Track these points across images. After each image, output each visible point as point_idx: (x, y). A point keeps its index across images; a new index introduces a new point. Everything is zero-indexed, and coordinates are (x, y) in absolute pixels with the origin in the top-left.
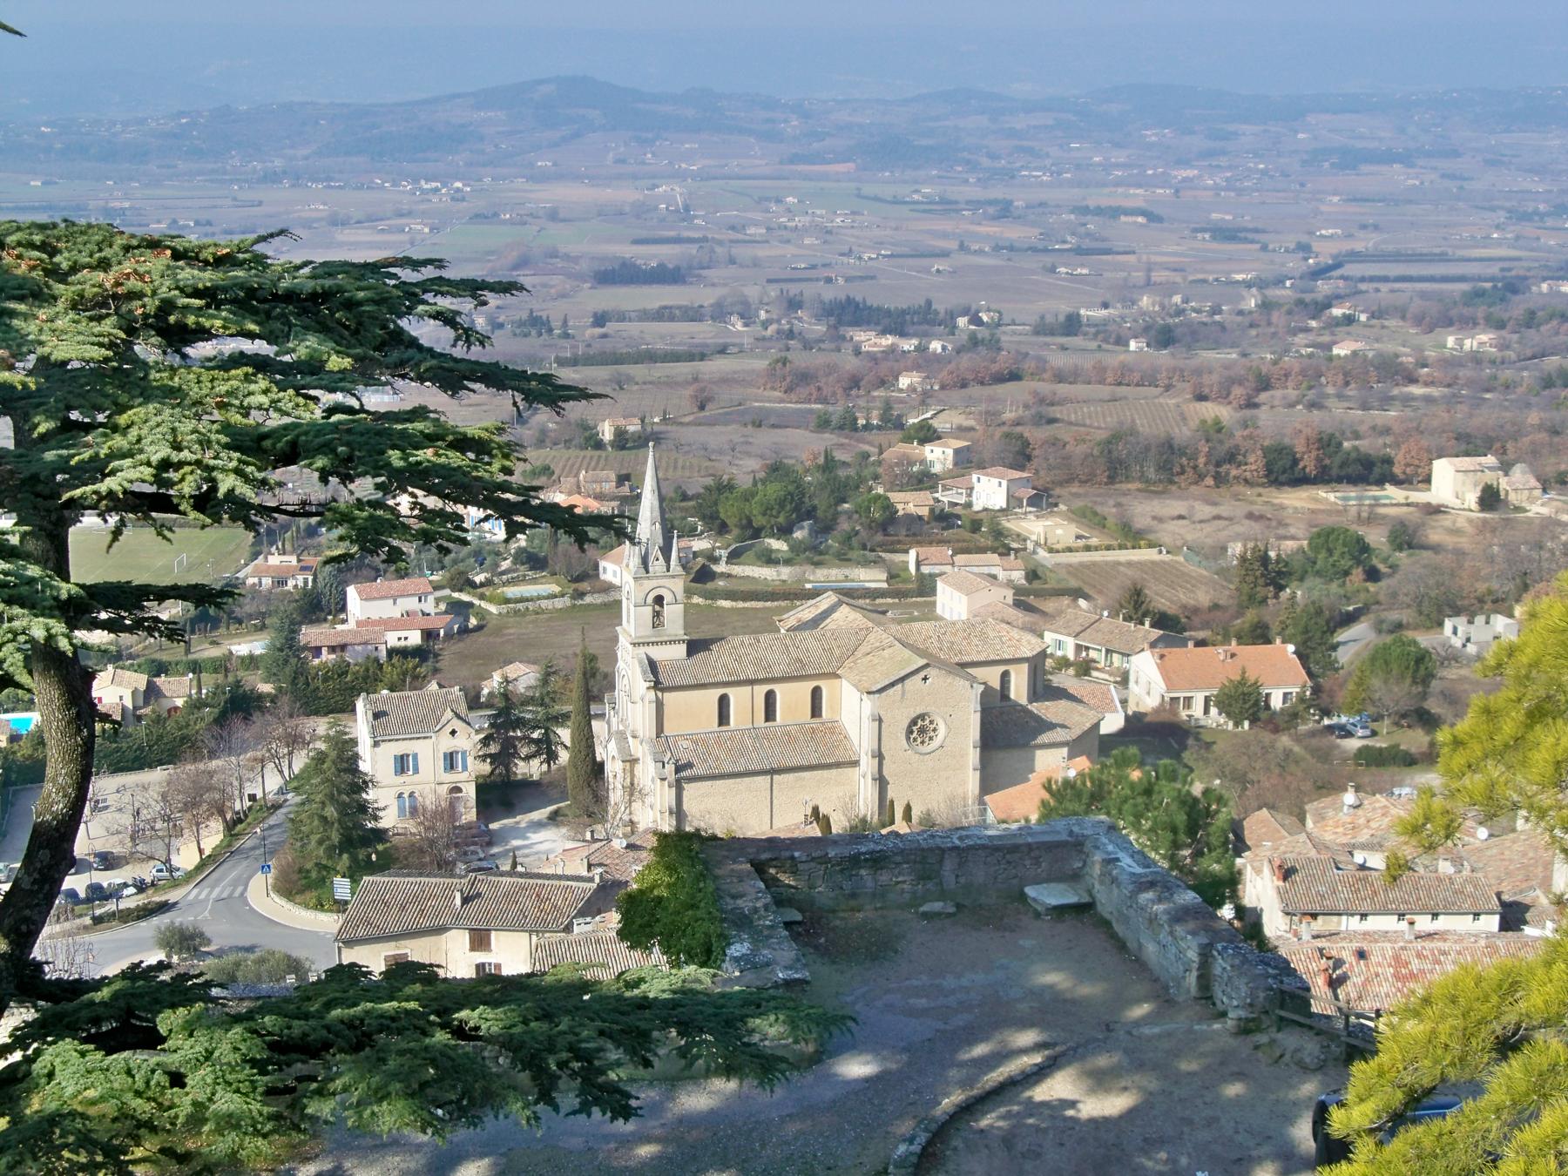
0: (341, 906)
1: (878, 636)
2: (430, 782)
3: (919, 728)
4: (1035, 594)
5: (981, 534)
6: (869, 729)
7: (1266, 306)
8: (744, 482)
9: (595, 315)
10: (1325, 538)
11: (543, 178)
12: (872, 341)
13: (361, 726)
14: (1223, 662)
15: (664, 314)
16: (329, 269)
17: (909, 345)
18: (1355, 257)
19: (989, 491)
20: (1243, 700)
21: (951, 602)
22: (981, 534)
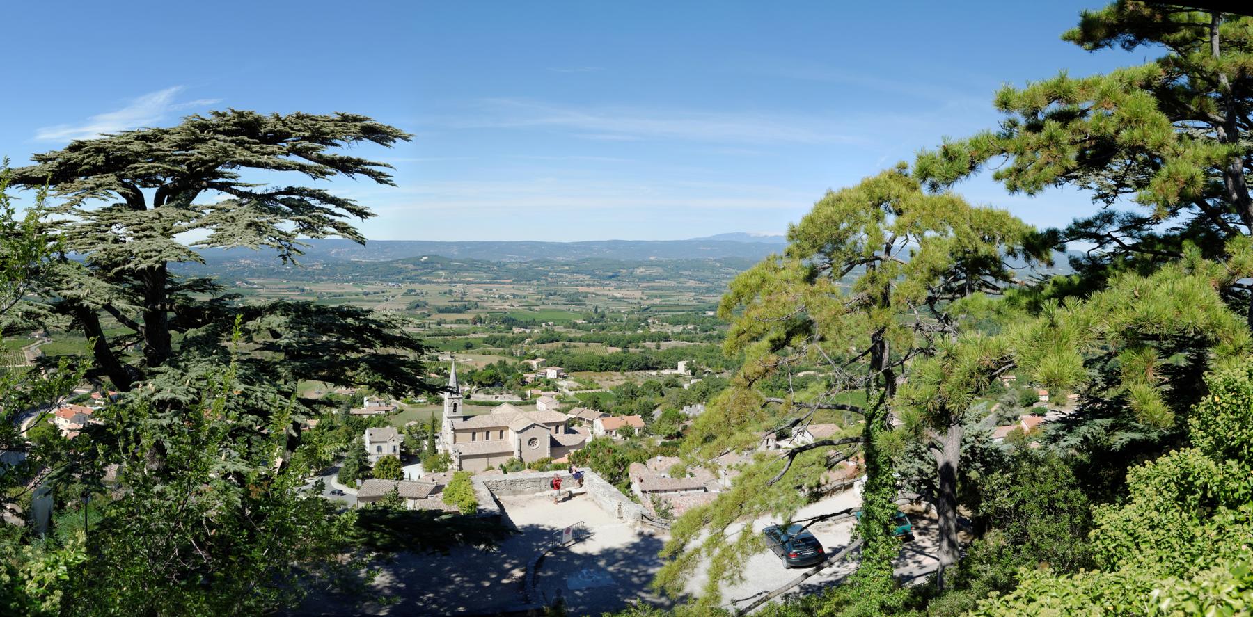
0: (359, 488)
1: (519, 415)
2: (387, 451)
3: (532, 441)
4: (565, 405)
5: (550, 385)
6: (517, 442)
7: (629, 320)
8: (480, 370)
9: (958, 353)
10: (649, 385)
11: (424, 282)
12: (517, 330)
13: (367, 438)
14: (618, 421)
15: (458, 322)
16: (77, 147)
17: (528, 331)
18: (654, 305)
19: (552, 373)
20: (627, 432)
21: (541, 405)
22: (550, 385)
